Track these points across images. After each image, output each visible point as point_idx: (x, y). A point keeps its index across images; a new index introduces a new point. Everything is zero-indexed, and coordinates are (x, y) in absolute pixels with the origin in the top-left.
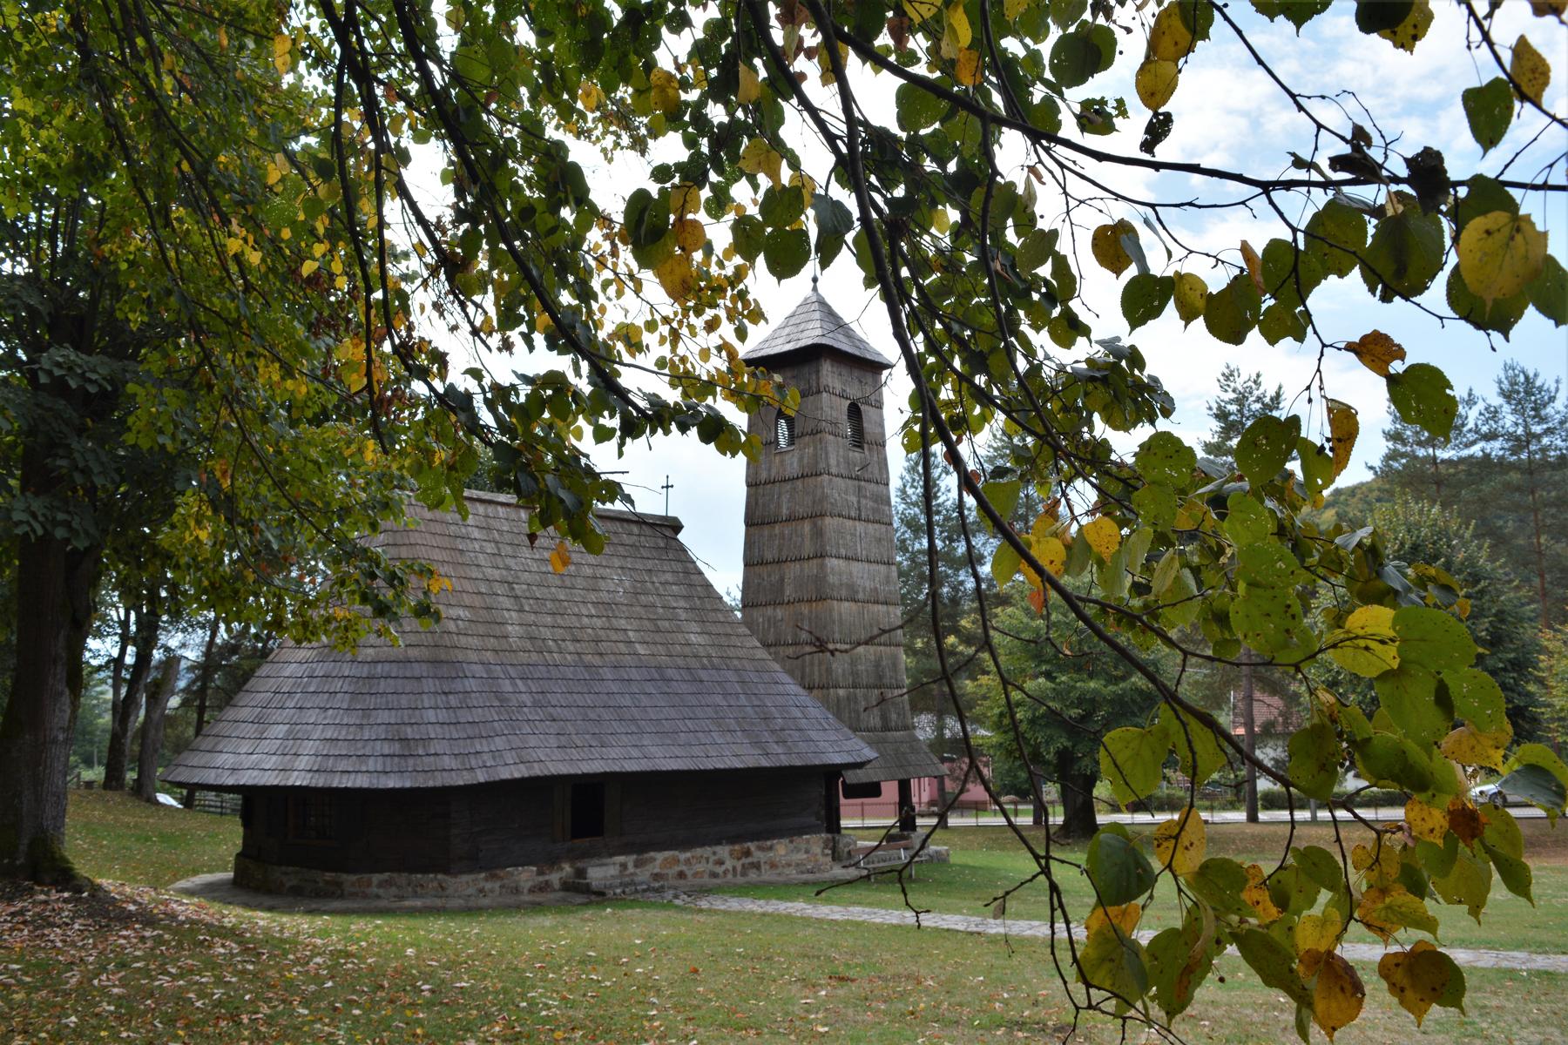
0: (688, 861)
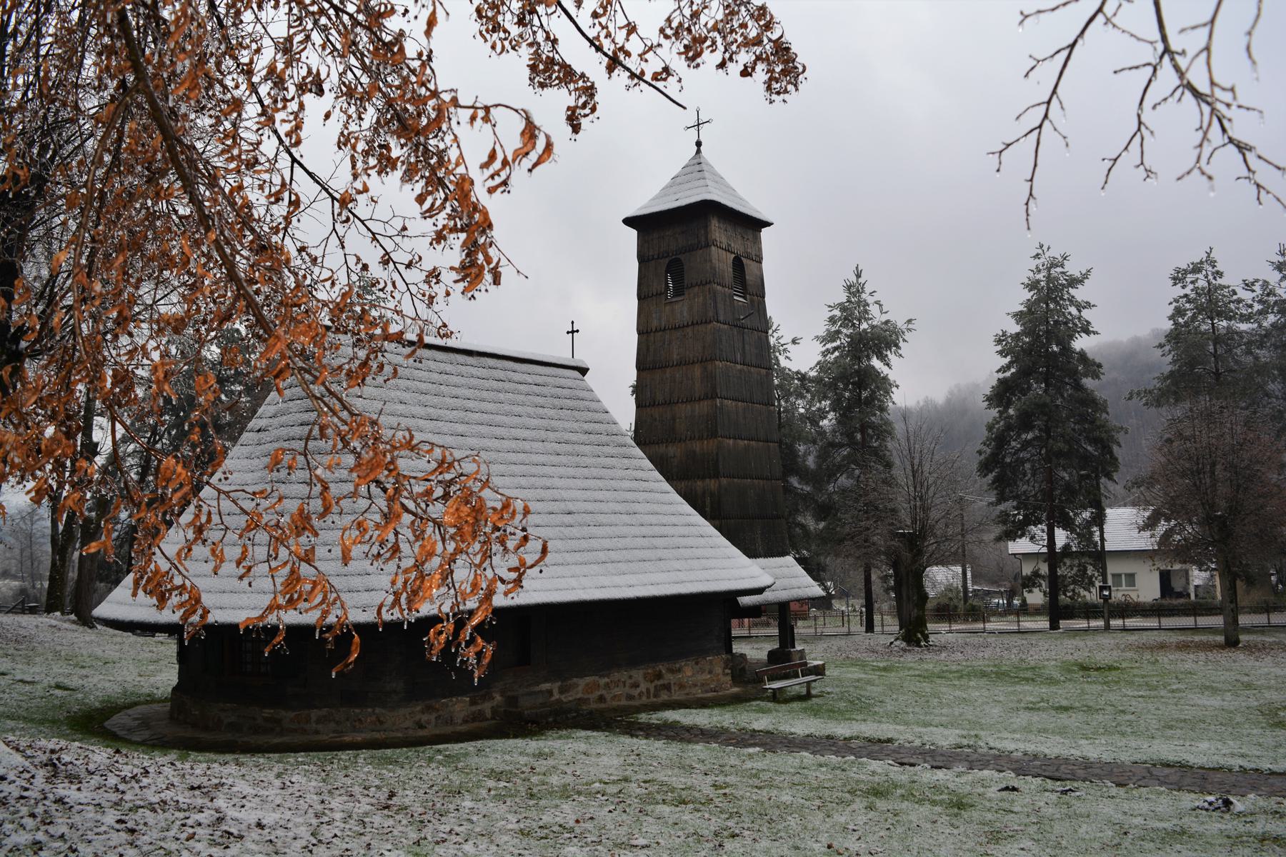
0: (607, 686)
